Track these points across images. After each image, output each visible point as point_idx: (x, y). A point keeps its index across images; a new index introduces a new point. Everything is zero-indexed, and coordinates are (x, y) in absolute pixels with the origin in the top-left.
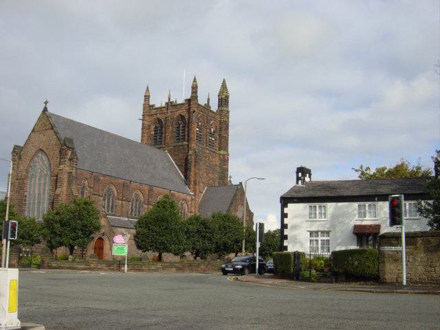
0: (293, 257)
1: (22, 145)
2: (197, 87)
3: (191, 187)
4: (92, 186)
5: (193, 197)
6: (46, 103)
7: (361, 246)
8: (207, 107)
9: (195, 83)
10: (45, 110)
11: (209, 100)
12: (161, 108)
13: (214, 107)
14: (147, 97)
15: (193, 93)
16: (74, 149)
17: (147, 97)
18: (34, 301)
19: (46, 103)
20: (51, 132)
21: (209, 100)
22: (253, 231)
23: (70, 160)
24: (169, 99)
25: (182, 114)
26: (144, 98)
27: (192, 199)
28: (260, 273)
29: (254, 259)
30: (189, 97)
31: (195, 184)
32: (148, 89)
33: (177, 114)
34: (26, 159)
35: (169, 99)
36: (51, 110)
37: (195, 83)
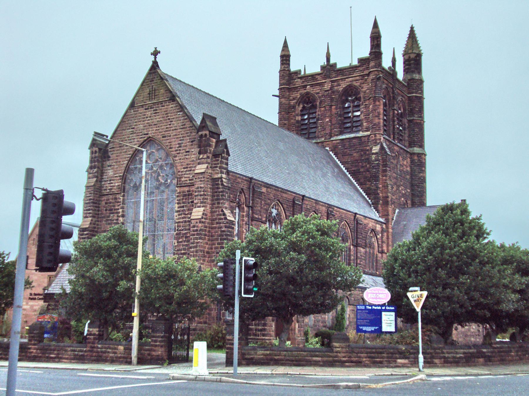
2: (289, 56)
6: (156, 53)
8: (392, 73)
10: (155, 66)
12: (313, 76)
13: (44, 192)
14: (285, 58)
15: (372, 47)
16: (219, 135)
17: (285, 58)
18: (393, 219)
19: (156, 53)
20: (171, 106)
22: (409, 288)
24: (328, 59)
25: (355, 83)
29: (386, 361)
32: (285, 45)
33: (343, 85)
35: (328, 59)
36: (164, 68)
37: (375, 30)
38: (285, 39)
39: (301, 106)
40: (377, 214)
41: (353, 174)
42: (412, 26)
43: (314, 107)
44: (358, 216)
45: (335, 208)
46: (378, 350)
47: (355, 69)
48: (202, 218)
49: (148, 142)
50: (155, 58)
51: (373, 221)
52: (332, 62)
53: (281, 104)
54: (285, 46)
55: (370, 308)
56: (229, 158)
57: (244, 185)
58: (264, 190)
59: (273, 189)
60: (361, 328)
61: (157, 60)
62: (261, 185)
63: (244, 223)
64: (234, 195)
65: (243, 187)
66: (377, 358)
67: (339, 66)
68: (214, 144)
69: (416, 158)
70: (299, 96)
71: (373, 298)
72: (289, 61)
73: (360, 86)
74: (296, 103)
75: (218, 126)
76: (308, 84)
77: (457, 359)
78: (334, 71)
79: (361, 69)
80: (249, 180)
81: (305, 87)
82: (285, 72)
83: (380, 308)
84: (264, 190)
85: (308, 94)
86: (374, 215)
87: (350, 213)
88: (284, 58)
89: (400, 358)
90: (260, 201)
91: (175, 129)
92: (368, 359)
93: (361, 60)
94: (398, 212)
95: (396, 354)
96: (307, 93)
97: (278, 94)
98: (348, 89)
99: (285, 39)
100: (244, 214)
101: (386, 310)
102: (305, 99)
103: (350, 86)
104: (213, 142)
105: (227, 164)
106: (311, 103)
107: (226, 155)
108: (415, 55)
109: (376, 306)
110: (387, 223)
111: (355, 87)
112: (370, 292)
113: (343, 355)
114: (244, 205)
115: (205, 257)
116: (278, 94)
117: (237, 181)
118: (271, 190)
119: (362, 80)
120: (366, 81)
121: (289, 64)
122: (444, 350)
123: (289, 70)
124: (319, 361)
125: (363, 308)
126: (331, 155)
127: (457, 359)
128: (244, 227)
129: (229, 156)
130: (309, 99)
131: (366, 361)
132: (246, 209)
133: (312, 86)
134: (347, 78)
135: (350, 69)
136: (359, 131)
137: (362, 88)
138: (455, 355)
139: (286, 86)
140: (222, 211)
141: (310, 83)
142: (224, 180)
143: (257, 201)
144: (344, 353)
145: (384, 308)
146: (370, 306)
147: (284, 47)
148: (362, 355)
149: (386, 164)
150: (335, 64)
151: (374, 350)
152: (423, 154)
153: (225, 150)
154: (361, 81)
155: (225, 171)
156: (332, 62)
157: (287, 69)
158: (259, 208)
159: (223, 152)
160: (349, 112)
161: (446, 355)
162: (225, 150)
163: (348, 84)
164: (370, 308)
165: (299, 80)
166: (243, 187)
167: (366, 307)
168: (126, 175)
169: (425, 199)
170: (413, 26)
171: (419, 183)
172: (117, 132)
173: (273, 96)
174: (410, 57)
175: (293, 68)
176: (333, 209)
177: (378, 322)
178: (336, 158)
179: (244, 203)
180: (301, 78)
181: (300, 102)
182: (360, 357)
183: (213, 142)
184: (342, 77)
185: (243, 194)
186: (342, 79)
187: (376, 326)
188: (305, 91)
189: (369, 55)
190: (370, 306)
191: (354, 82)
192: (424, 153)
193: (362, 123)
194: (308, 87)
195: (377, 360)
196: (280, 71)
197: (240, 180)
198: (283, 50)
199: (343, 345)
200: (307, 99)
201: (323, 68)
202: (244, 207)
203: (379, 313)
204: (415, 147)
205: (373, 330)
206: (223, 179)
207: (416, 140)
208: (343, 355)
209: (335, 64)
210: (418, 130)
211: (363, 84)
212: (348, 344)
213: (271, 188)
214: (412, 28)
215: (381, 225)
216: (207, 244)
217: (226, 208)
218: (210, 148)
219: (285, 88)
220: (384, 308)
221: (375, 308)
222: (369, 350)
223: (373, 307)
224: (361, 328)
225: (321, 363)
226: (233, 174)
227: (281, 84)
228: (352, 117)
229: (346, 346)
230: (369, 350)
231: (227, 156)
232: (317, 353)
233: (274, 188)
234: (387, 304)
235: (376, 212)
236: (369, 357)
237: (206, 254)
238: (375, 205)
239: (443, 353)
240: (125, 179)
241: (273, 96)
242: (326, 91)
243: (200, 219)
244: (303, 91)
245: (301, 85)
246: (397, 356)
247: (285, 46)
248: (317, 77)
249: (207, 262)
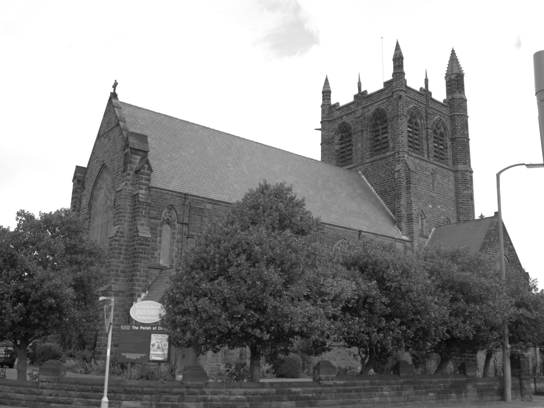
0: (111, 388)
1: (85, 165)
2: (330, 92)
3: (403, 225)
4: (186, 220)
5: (408, 244)
7: (182, 404)
8: (425, 93)
9: (398, 52)
10: (114, 95)
11: (426, 81)
12: (347, 106)
14: (326, 93)
17: (326, 93)
21: (426, 81)
23: (137, 172)
26: (321, 95)
27: (406, 248)
28: (520, 389)
30: (390, 77)
31: (410, 220)
33: (372, 109)
34: (89, 186)
36: (121, 98)
38: (327, 77)
39: (340, 135)
40: (400, 232)
41: (381, 194)
42: (453, 49)
43: (350, 135)
44: (362, 233)
45: (326, 226)
46: (94, 387)
47: (381, 93)
48: (116, 236)
49: (104, 168)
50: (115, 90)
51: (390, 239)
52: (363, 90)
53: (322, 135)
54: (327, 82)
55: (137, 328)
56: (152, 174)
57: (177, 202)
58: (209, 206)
59: (222, 205)
60: (124, 354)
61: (116, 91)
62: (202, 201)
63: (175, 240)
64: (159, 211)
65: (173, 203)
66: (92, 398)
67: (369, 93)
68: (138, 161)
69: (459, 175)
70: (337, 127)
71: (142, 316)
72: (330, 96)
73: (386, 108)
74: (335, 133)
75: (147, 143)
76: (344, 114)
77: (230, 403)
78: (365, 98)
79: (386, 91)
80: (184, 196)
81: (342, 117)
82: (325, 106)
83: (149, 328)
84: (209, 206)
85: (344, 124)
86: (394, 232)
87: (352, 231)
88: (325, 94)
89: (126, 400)
90: (199, 217)
91: (118, 152)
92: (80, 399)
93: (386, 84)
94: (434, 231)
95: (121, 393)
96: (344, 123)
97: (320, 127)
98: (376, 113)
99: (327, 77)
100: (175, 231)
101: (157, 332)
102: (343, 129)
103: (378, 110)
104: (136, 159)
105: (149, 180)
106: (347, 131)
107: (146, 171)
108: (456, 75)
109: (144, 325)
110: (411, 242)
111: (383, 110)
112: (139, 307)
113: (50, 392)
114: (175, 221)
115: (118, 276)
116: (320, 127)
117: (164, 197)
118: (221, 206)
119: (387, 102)
120: (391, 102)
121: (330, 99)
122: (205, 390)
123: (330, 104)
124: (22, 400)
125: (127, 328)
126: (362, 179)
127: (230, 403)
128: (175, 245)
129: (152, 171)
130: (346, 129)
131: (77, 401)
132: (178, 226)
133: (347, 115)
134: (375, 103)
135: (377, 94)
136: (387, 152)
137: (388, 110)
138: (226, 397)
139: (326, 119)
140: (136, 228)
141: (346, 113)
142: (140, 196)
143: (194, 217)
144: (51, 389)
145: (155, 328)
146: (136, 326)
147: (325, 84)
148: (73, 393)
149: (410, 181)
150: (366, 91)
151: (90, 388)
152: (467, 171)
153: (146, 166)
154: (387, 103)
155: (144, 187)
156: (363, 90)
157: (326, 104)
158: (199, 225)
159: (143, 167)
160: (379, 135)
161: (209, 397)
162: (146, 166)
163: (376, 108)
164: (137, 328)
165: (337, 112)
166: (173, 203)
167: (131, 328)
168: (91, 202)
169: (474, 216)
170: (454, 49)
171: (464, 201)
172: (90, 163)
173: (315, 129)
174: (450, 79)
175: (333, 102)
176: (324, 227)
177: (146, 347)
178: (366, 181)
179: (175, 220)
180: (338, 110)
181: (338, 132)
182: (69, 396)
183: (136, 159)
184: (371, 103)
185: (173, 210)
186: (370, 105)
187: (142, 353)
188: (342, 121)
189: (392, 78)
190: (136, 326)
191: (382, 105)
192: (469, 169)
193: (389, 144)
194: (344, 117)
195: (93, 400)
196: (322, 106)
197: (169, 197)
198: (324, 87)
199: (50, 377)
200: (345, 129)
201: (356, 96)
202: (175, 224)
203: (147, 336)
204: (458, 164)
205: (139, 357)
206: (140, 195)
207: (459, 157)
208: (50, 392)
209: (366, 91)
210: (461, 148)
211: (389, 105)
212: (56, 377)
213: (219, 205)
214: (453, 51)
215: (403, 243)
216: (122, 263)
217: (142, 225)
218: (131, 165)
219: (325, 121)
220: (155, 328)
221: (144, 328)
222: (83, 387)
223: (141, 327)
224: (124, 354)
225: (24, 402)
226: (157, 190)
227: (322, 118)
228: (381, 139)
229: (55, 379)
230: (83, 387)
231: (150, 172)
232: (21, 388)
233: (224, 204)
234: (160, 324)
235: (399, 230)
236: (83, 397)
237: (120, 273)
238: (396, 222)
239: (203, 393)
240: (91, 206)
241: (315, 129)
242: (358, 118)
243: (113, 237)
244: (340, 122)
245: (339, 116)
246: (123, 396)
247: (327, 82)
248: (351, 106)
249: (122, 281)
